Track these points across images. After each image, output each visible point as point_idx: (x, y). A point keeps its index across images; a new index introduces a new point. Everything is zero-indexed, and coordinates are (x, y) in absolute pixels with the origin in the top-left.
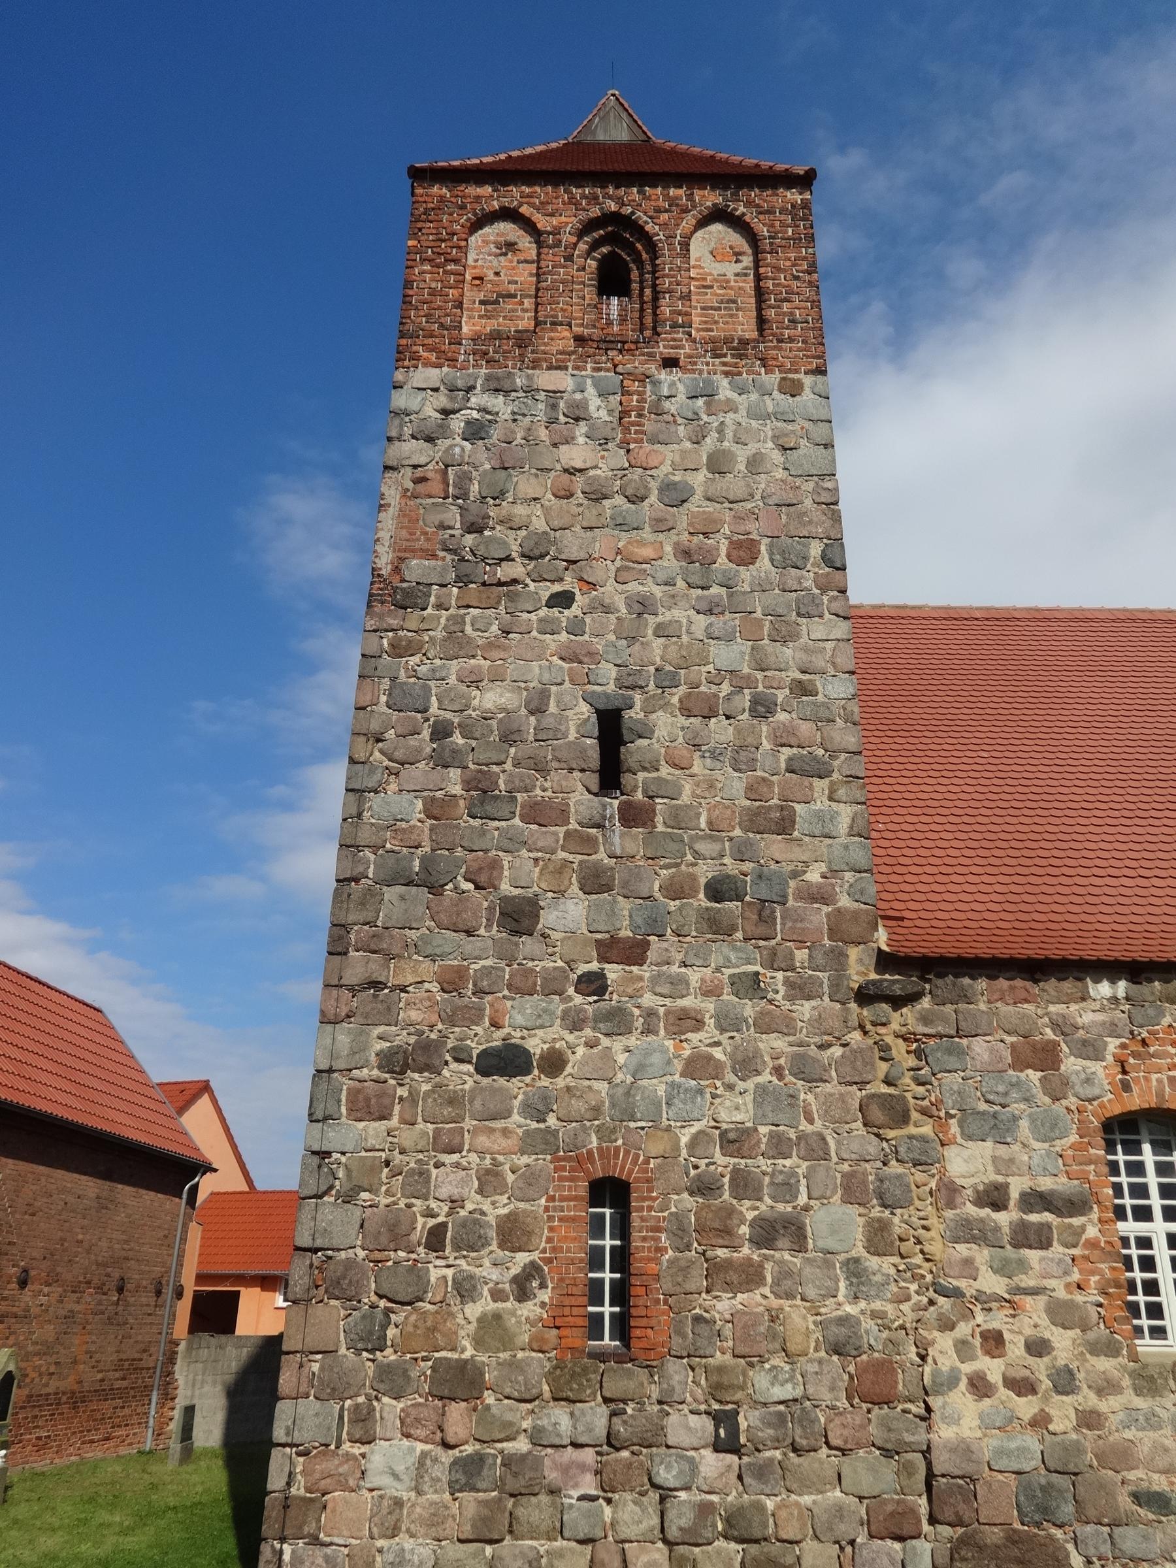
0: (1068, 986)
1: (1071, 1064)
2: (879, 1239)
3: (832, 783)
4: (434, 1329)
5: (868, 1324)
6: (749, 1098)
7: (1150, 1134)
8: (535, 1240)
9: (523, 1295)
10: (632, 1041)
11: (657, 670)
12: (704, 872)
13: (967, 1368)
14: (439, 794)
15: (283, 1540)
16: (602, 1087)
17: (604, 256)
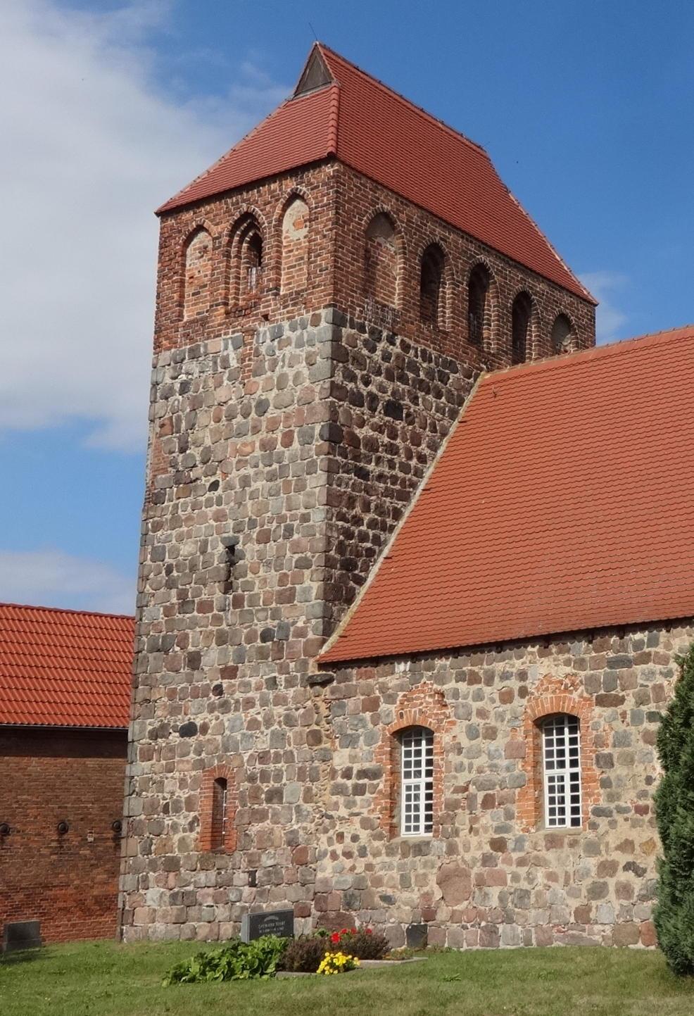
0: (387, 668)
1: (384, 707)
2: (308, 797)
3: (312, 571)
4: (165, 845)
5: (301, 832)
6: (269, 736)
7: (569, 723)
8: (196, 807)
9: (191, 830)
10: (230, 715)
11: (249, 519)
12: (260, 628)
13: (330, 849)
14: (168, 604)
15: (123, 925)
16: (219, 738)
17: (251, 238)
